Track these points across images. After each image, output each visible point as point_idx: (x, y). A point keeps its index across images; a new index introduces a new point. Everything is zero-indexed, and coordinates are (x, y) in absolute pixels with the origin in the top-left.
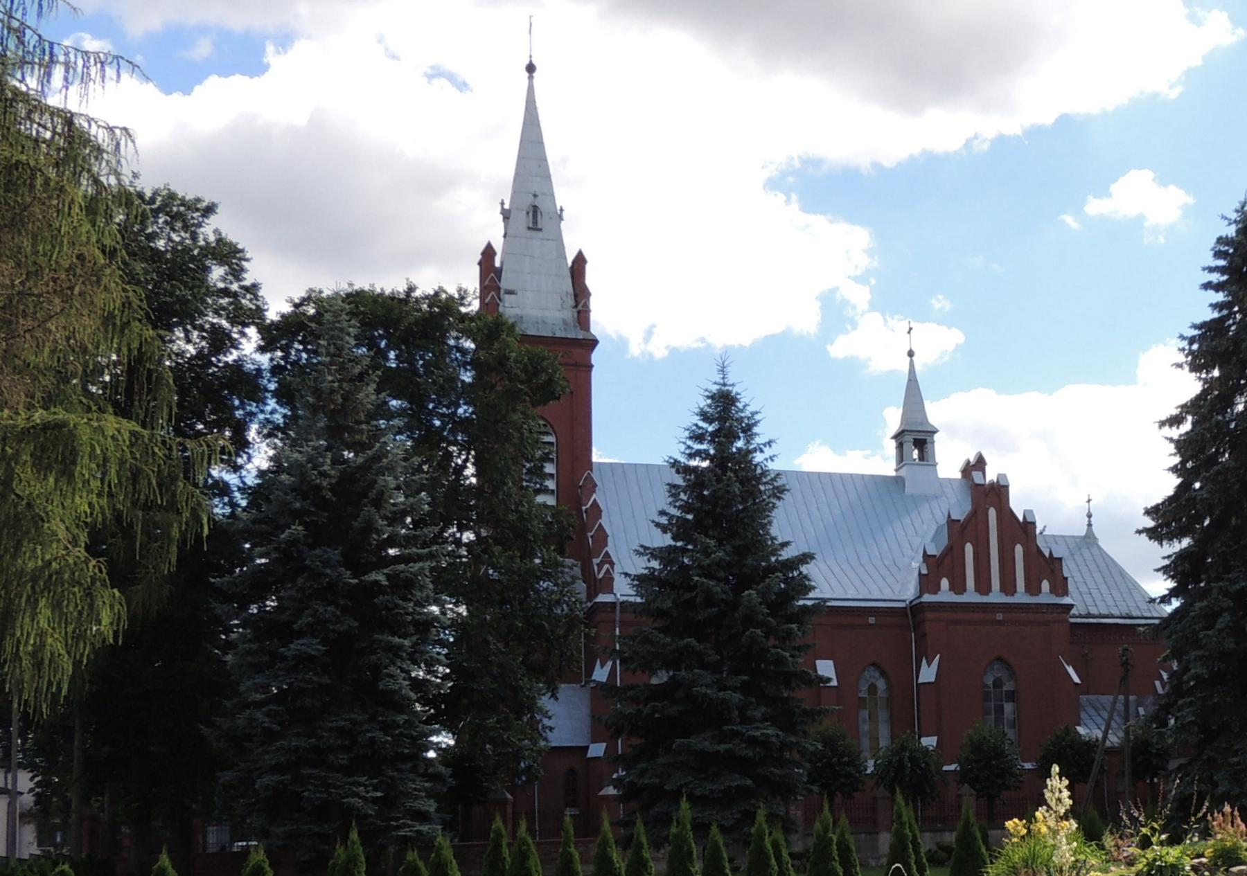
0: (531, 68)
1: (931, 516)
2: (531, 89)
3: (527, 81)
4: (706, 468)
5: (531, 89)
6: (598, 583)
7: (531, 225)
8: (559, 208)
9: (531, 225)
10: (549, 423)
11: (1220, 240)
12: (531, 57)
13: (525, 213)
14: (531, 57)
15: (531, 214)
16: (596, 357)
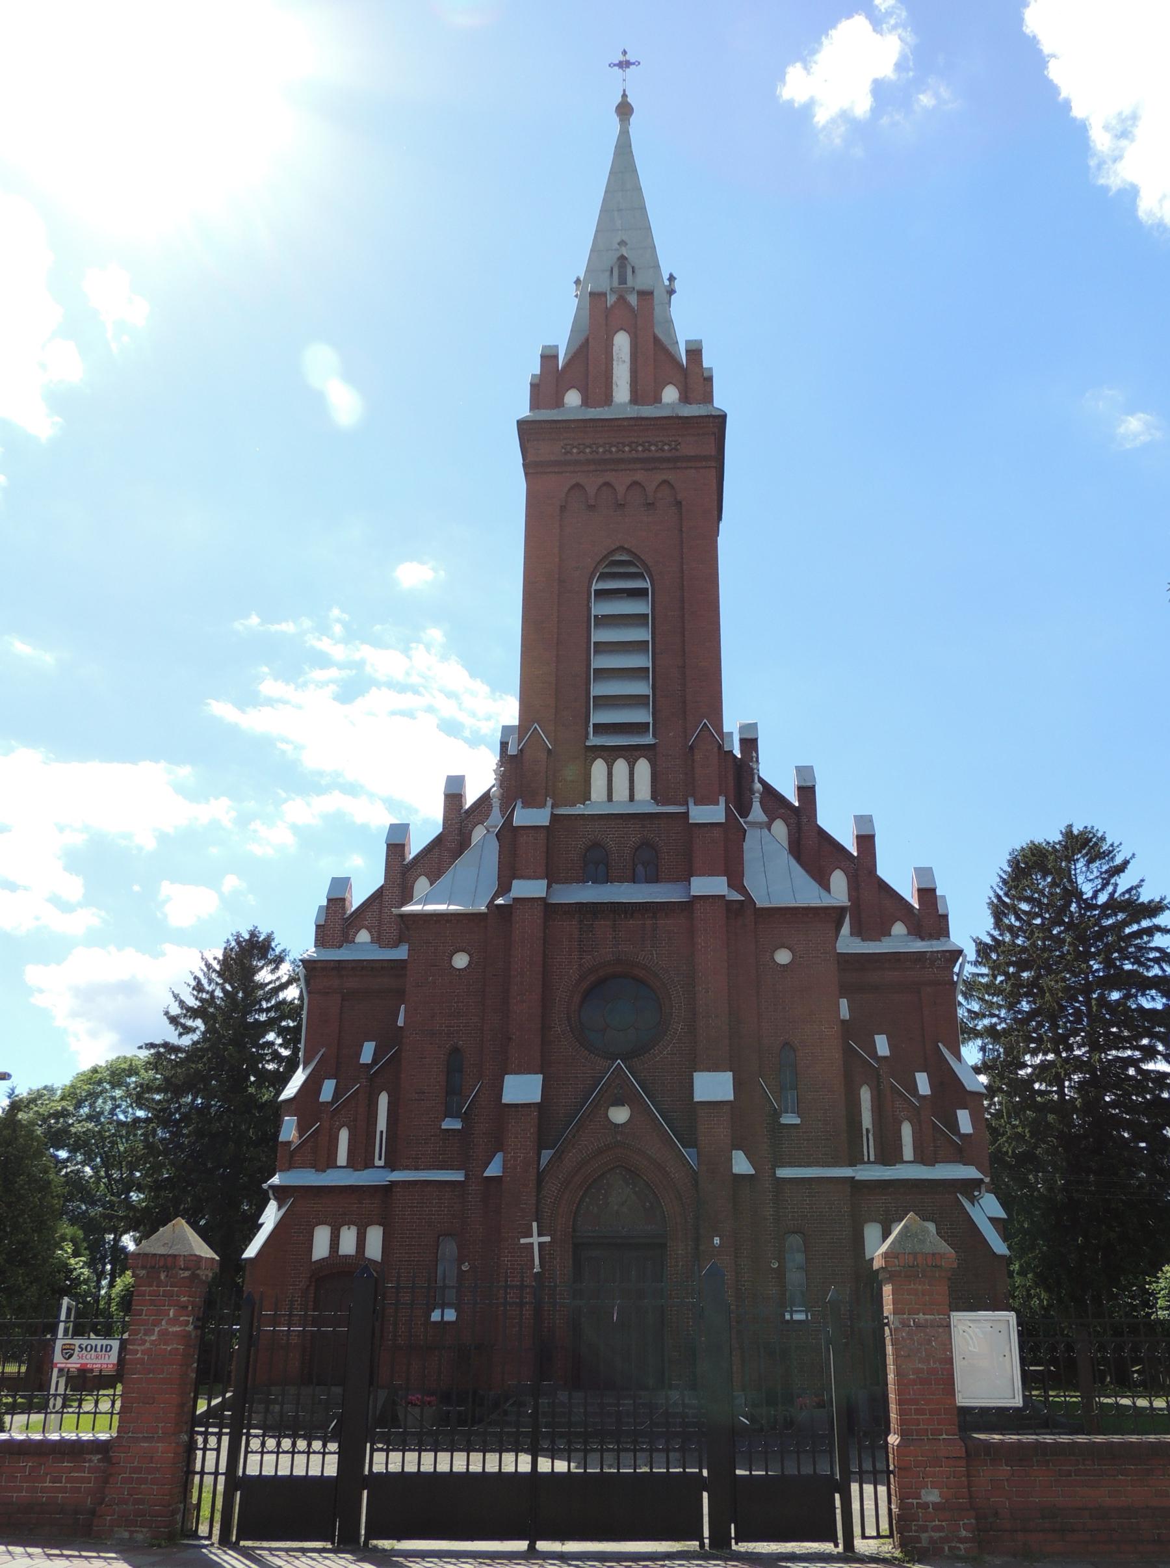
2: (624, 136)
5: (624, 136)
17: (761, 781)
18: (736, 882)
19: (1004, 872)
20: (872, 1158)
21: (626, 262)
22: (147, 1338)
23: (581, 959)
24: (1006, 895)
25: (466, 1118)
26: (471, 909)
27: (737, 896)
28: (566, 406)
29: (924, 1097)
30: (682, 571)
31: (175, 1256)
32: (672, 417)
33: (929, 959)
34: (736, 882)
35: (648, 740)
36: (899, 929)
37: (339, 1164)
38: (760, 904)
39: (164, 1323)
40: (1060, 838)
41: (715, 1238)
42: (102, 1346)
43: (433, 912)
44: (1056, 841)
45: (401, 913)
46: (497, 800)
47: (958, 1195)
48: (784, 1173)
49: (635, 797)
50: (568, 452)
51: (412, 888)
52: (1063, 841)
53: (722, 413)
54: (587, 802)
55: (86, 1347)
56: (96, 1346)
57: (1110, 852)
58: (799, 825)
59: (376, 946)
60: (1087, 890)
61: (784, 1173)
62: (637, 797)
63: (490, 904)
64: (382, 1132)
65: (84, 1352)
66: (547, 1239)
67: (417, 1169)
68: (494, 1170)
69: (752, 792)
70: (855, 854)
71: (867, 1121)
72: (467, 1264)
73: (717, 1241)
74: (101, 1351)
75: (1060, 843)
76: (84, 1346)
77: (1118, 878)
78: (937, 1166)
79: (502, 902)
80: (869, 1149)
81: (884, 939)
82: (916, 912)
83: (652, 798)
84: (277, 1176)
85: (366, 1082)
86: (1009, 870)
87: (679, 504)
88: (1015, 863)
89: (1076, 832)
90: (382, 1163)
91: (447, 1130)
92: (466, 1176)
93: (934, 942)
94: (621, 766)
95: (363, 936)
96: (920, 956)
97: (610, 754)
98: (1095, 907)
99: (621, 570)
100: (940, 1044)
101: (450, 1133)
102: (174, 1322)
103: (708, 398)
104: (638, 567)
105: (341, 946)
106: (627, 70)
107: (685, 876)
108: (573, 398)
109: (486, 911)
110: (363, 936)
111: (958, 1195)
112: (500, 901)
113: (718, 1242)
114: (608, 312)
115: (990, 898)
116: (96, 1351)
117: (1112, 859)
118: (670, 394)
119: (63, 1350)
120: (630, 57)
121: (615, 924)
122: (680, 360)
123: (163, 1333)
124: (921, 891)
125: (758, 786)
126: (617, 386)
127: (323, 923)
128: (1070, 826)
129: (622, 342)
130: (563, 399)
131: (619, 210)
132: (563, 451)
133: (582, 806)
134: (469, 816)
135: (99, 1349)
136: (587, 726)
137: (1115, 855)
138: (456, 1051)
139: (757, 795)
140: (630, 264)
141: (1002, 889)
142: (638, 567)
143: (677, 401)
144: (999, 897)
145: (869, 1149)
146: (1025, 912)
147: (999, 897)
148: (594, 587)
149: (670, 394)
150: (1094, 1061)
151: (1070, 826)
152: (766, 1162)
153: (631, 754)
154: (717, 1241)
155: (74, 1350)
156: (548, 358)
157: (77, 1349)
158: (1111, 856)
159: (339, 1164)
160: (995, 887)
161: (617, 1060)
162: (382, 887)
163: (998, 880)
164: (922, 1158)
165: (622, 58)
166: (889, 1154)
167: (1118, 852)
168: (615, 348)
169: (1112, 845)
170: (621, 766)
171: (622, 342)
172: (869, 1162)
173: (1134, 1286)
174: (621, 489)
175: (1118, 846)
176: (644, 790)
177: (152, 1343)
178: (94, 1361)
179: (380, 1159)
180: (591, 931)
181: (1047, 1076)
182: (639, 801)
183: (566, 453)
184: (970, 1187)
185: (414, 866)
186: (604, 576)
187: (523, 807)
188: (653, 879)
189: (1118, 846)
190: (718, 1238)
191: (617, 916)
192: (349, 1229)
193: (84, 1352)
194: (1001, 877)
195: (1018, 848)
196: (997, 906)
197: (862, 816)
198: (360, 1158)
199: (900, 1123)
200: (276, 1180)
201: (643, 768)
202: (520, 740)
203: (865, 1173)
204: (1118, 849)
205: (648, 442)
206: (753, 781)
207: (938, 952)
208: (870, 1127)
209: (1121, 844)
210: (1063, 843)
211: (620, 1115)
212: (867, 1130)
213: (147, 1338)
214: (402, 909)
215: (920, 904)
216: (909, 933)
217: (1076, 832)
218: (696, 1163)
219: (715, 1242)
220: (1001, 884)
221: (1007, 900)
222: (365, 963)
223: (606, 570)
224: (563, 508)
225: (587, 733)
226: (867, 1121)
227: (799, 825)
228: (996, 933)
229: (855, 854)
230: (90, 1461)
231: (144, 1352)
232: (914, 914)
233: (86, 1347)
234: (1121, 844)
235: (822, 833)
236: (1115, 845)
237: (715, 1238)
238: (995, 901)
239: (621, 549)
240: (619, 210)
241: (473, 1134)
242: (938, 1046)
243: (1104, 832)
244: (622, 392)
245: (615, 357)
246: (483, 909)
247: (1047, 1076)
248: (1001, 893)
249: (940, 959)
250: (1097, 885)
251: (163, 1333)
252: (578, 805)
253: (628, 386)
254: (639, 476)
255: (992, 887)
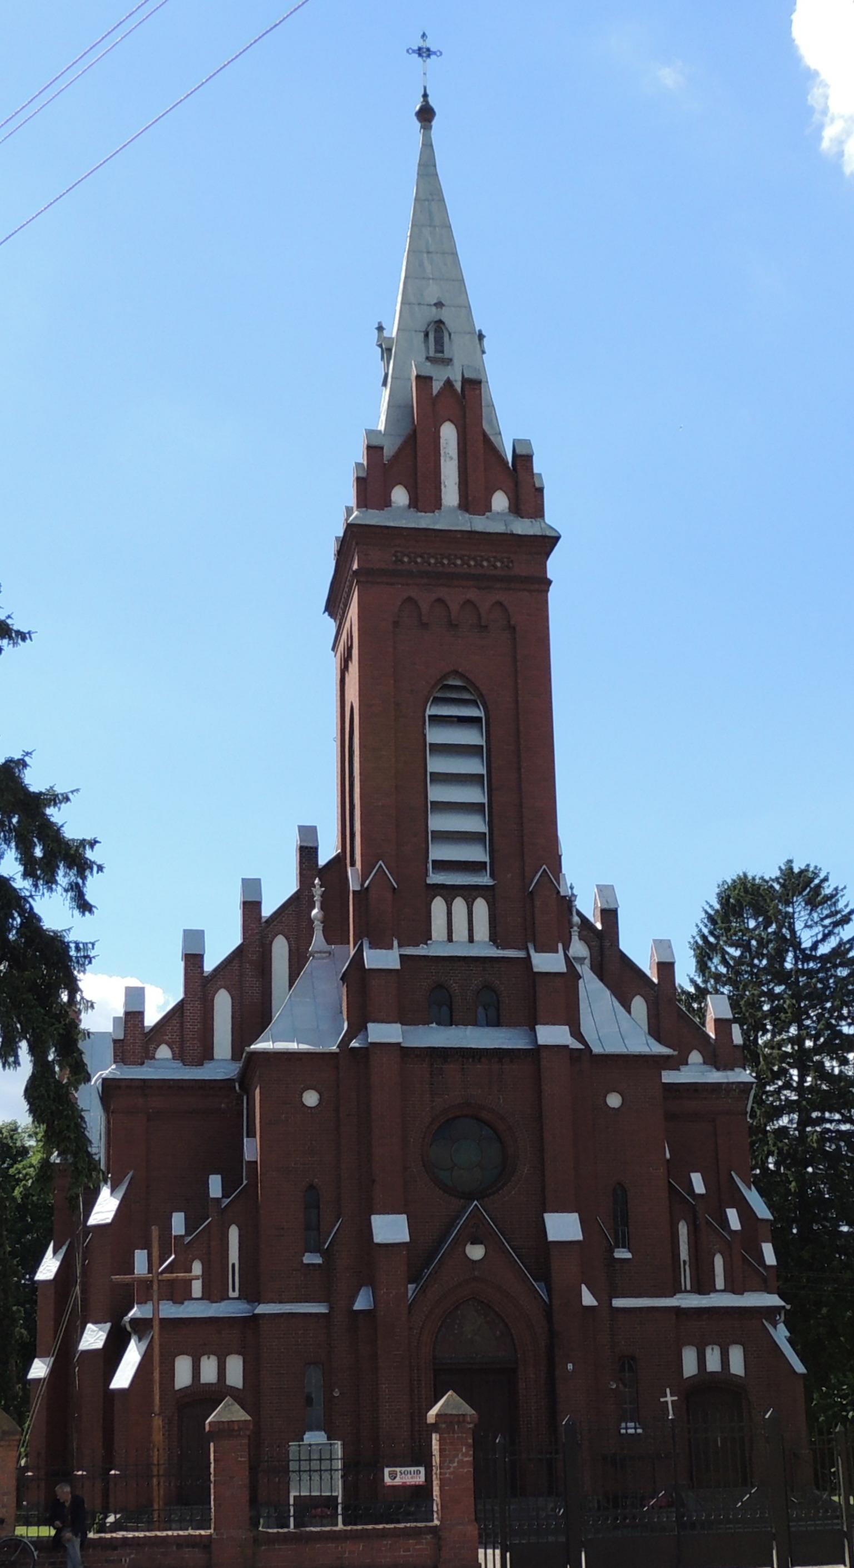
0: (426, 114)
1: (597, 1037)
2: (428, 146)
3: (420, 138)
4: (33, 853)
5: (428, 146)
6: (112, 1485)
7: (432, 354)
8: (569, 885)
9: (432, 354)
10: (473, 684)
11: (15, 644)
12: (425, 96)
13: (422, 335)
14: (425, 96)
15: (431, 336)
16: (555, 565)
17: (579, 914)
18: (577, 1033)
19: (711, 906)
20: (688, 1288)
21: (443, 328)
22: (451, 1465)
23: (433, 1101)
24: (711, 933)
25: (326, 1254)
26: (320, 1049)
27: (576, 1045)
28: (393, 505)
29: (736, 1231)
30: (517, 702)
31: (464, 1415)
32: (507, 534)
33: (725, 1090)
34: (577, 1033)
35: (484, 880)
36: (695, 1057)
37: (194, 1295)
38: (597, 1049)
39: (460, 1455)
40: (778, 874)
41: (569, 1365)
42: (414, 1471)
43: (285, 1051)
44: (773, 877)
45: (251, 1050)
46: (319, 923)
47: (764, 1321)
48: (618, 1303)
49: (475, 938)
50: (400, 561)
51: (213, 1000)
52: (781, 877)
53: (553, 534)
54: (429, 942)
55: (404, 1472)
56: (410, 1471)
57: (832, 896)
58: (602, 948)
59: (178, 1064)
60: (807, 939)
61: (618, 1303)
62: (476, 938)
63: (344, 1043)
64: (233, 1265)
65: (403, 1475)
66: (662, 1400)
67: (281, 1302)
68: (362, 1302)
69: (571, 926)
70: (655, 980)
71: (684, 1254)
72: (337, 1390)
73: (570, 1366)
74: (414, 1473)
75: (777, 879)
76: (402, 1472)
77: (841, 930)
78: (746, 1294)
79: (357, 1045)
80: (687, 1281)
81: (683, 1068)
82: (713, 1042)
83: (490, 940)
84: (135, 1309)
85: (217, 1216)
86: (717, 906)
87: (513, 629)
88: (724, 899)
89: (796, 870)
90: (236, 1294)
91: (308, 1265)
92: (331, 1308)
93: (729, 1073)
94: (459, 905)
95: (164, 1052)
96: (716, 1087)
97: (449, 892)
98: (814, 958)
99: (454, 696)
100: (733, 1173)
101: (311, 1268)
102: (466, 1455)
103: (538, 512)
104: (471, 693)
105: (142, 1064)
106: (428, 60)
107: (531, 1024)
108: (400, 496)
109: (338, 1050)
110: (164, 1052)
111: (764, 1321)
112: (354, 1044)
113: (571, 1368)
114: (435, 401)
115: (694, 937)
116: (411, 1474)
117: (835, 904)
118: (500, 501)
119: (390, 1474)
120: (430, 44)
121: (463, 1068)
122: (500, 449)
123: (460, 1462)
124: (603, 912)
125: (576, 919)
126: (445, 486)
127: (122, 1037)
128: (790, 861)
129: (448, 433)
130: (390, 496)
131: (428, 252)
132: (394, 558)
133: (425, 946)
134: (270, 925)
135: (412, 1472)
136: (427, 862)
137: (838, 900)
138: (312, 1187)
139: (575, 928)
140: (447, 329)
141: (706, 926)
142: (471, 693)
143: (507, 510)
144: (704, 938)
145: (687, 1281)
146: (733, 958)
147: (704, 938)
148: (428, 713)
149: (500, 501)
150: (812, 1140)
151: (790, 861)
152: (606, 1292)
153: (469, 893)
154: (570, 1366)
155: (396, 1474)
156: (373, 450)
157: (399, 1474)
158: (834, 900)
159: (194, 1295)
160: (701, 926)
161: (474, 1201)
162: (182, 1001)
163: (703, 915)
164: (733, 1287)
165: (421, 43)
166: (703, 1285)
167: (842, 896)
168: (442, 441)
169: (836, 889)
170: (459, 905)
171: (448, 433)
172: (686, 1291)
173: (844, 1385)
174: (454, 608)
175: (842, 890)
176: (482, 930)
177: (454, 1467)
178: (411, 1480)
179: (234, 1290)
180: (442, 1075)
181: (758, 1155)
182: (479, 942)
183: (395, 562)
184: (770, 1313)
185: (214, 977)
186: (438, 701)
187: (371, 948)
188: (496, 1022)
189: (842, 890)
190: (571, 1365)
191: (465, 1060)
192: (209, 1358)
193: (403, 1475)
194: (706, 912)
195: (729, 881)
196: (702, 949)
197: (661, 941)
198: (214, 1292)
199: (714, 1255)
200: (135, 1312)
201: (481, 907)
202: (364, 877)
203: (687, 1301)
204: (842, 893)
205: (481, 557)
206: (571, 914)
207: (733, 1083)
208: (687, 1258)
209: (845, 888)
210: (781, 881)
211: (476, 1252)
212: (684, 1261)
213: (451, 1465)
214: (252, 1047)
215: (716, 1035)
216: (705, 1063)
217: (796, 870)
218: (546, 1293)
219: (569, 1368)
220: (706, 921)
221: (712, 939)
222: (171, 1082)
223: (439, 695)
224: (396, 624)
225: (427, 870)
226: (684, 1254)
227: (602, 948)
228: (699, 981)
229: (655, 980)
230: (426, 1538)
231: (450, 1473)
232: (710, 1043)
233: (404, 1472)
234: (845, 888)
235: (623, 957)
236: (840, 888)
237: (569, 1365)
238: (700, 942)
239: (456, 673)
240: (428, 252)
241: (335, 1269)
242: (731, 1175)
243: (828, 873)
244: (450, 495)
245: (442, 452)
246: (334, 1048)
247: (758, 1155)
248: (706, 931)
249: (735, 1090)
250: (817, 934)
251: (460, 1462)
252: (421, 945)
253: (456, 488)
254: (472, 595)
255: (697, 926)
